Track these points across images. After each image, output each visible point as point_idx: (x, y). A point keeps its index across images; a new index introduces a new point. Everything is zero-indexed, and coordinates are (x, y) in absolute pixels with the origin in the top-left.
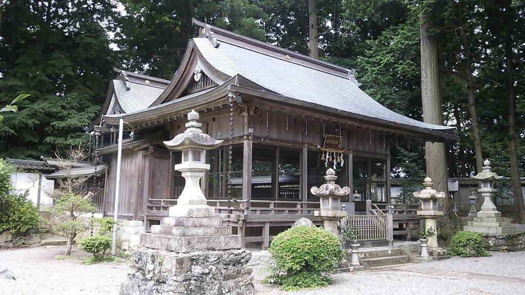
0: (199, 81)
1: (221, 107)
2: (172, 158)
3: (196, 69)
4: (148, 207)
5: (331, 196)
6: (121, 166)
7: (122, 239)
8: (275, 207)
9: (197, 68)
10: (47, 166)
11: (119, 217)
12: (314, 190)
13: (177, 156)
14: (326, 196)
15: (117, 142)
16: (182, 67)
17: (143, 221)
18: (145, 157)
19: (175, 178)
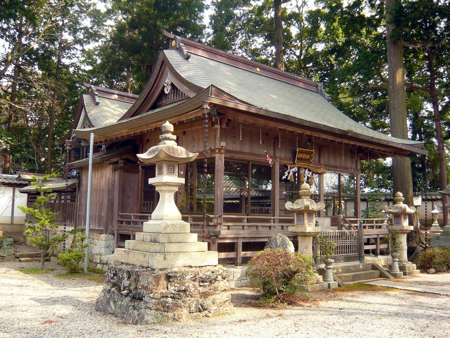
0: (169, 93)
1: (193, 120)
2: (142, 172)
3: (166, 82)
4: (118, 221)
5: (306, 211)
6: (92, 179)
7: (94, 252)
8: (248, 222)
9: (167, 81)
10: (20, 180)
11: (91, 230)
12: (289, 205)
13: (150, 170)
14: (301, 211)
15: (87, 156)
16: (152, 80)
17: (114, 235)
18: (115, 170)
19: (145, 192)
